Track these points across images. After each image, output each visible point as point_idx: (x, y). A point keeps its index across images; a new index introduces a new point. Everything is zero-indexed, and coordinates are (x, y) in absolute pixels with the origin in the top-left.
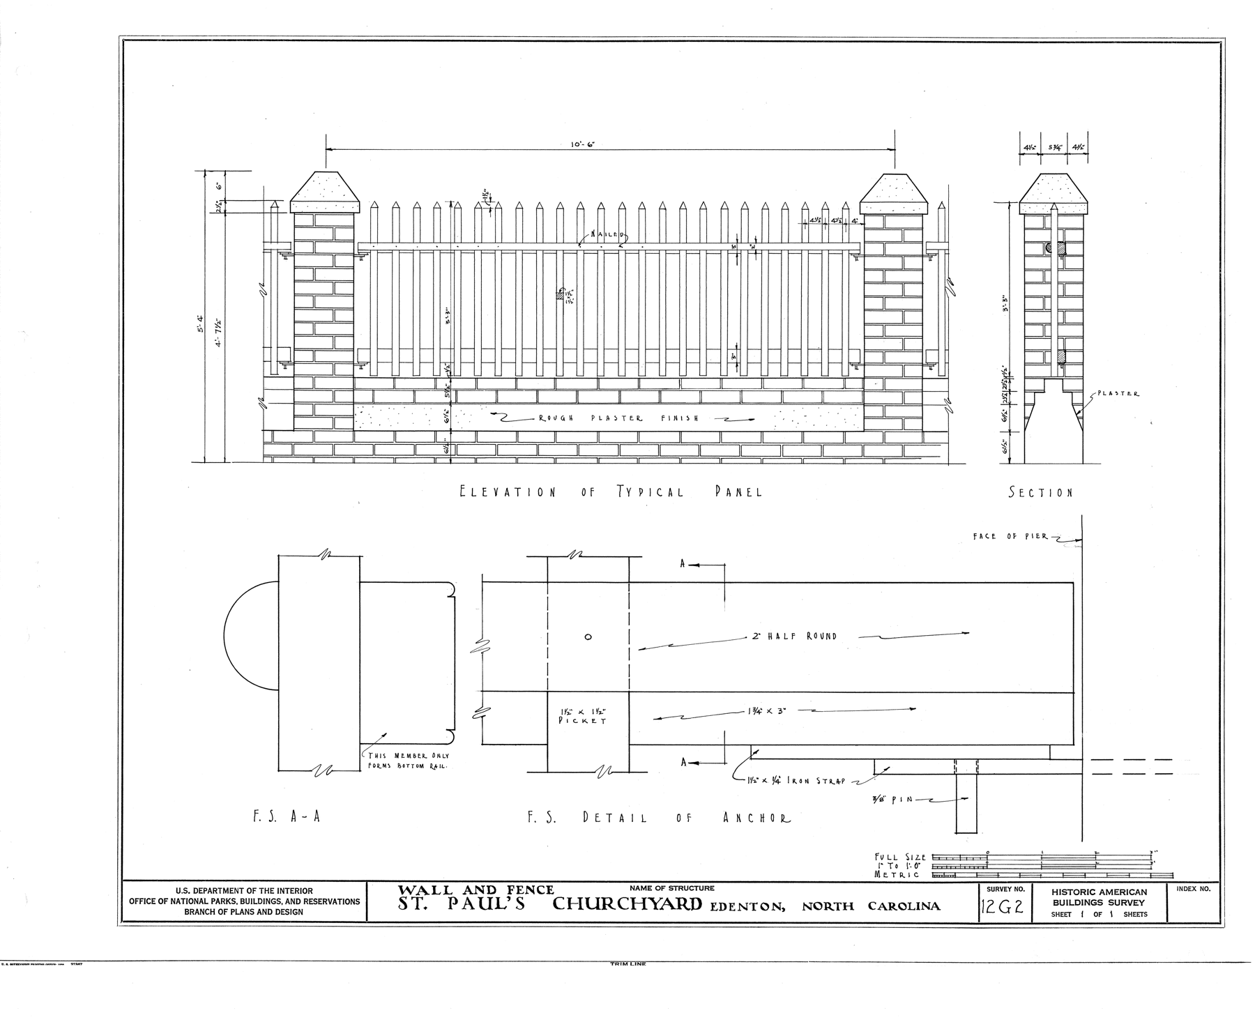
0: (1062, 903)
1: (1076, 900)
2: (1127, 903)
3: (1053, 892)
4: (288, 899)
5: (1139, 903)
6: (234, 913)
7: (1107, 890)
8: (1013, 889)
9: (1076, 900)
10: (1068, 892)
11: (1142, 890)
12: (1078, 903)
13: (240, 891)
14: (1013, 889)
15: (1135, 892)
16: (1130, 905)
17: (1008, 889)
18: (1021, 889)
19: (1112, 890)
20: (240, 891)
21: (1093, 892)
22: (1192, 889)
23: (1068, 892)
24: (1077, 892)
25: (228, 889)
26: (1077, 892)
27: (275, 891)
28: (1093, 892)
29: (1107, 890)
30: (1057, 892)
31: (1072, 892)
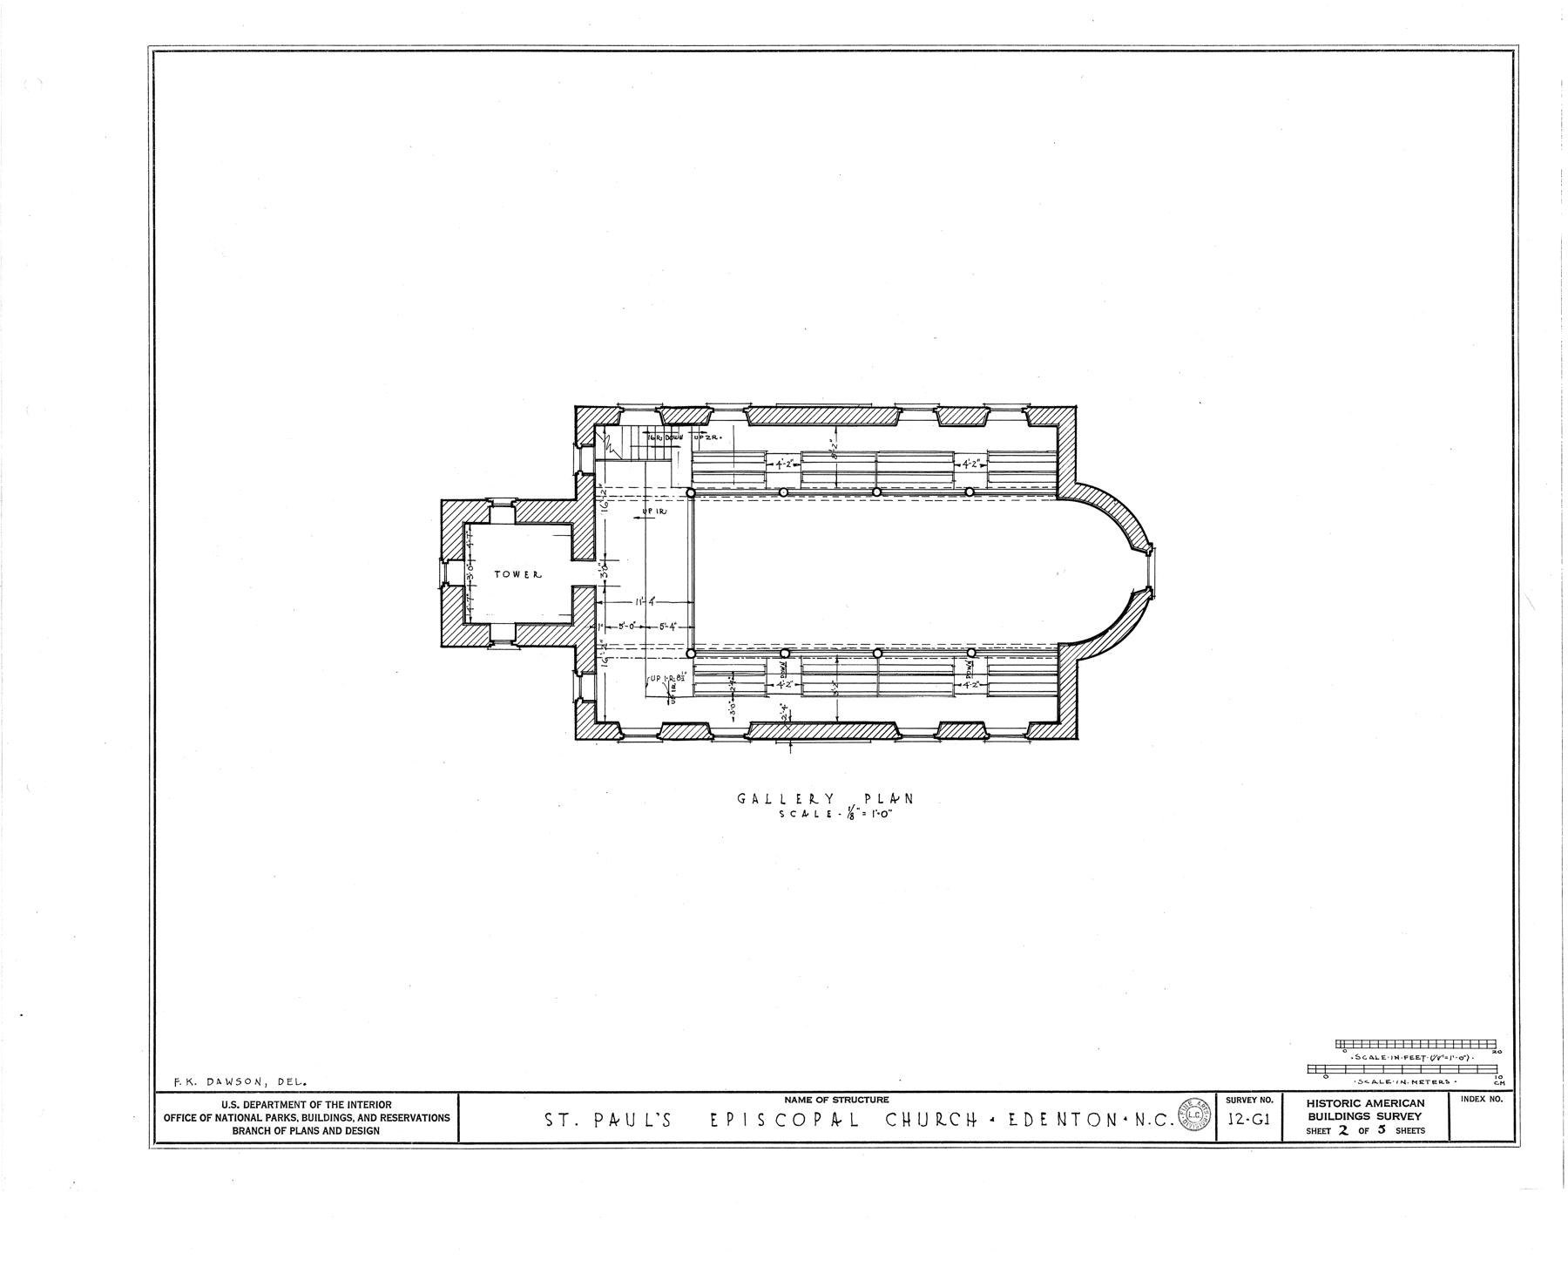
0: (1320, 1117)
4: (326, 1128)
5: (1415, 1117)
8: (1258, 1100)
10: (1327, 1103)
11: (1419, 1101)
12: (1339, 1116)
13: (301, 1104)
14: (1258, 1100)
15: (1410, 1103)
16: (1404, 1119)
17: (1252, 1100)
19: (1381, 1101)
20: (301, 1104)
21: (1357, 1103)
25: (286, 1102)
26: (1337, 1103)
28: (1357, 1103)
29: (1375, 1101)
30: (1313, 1103)
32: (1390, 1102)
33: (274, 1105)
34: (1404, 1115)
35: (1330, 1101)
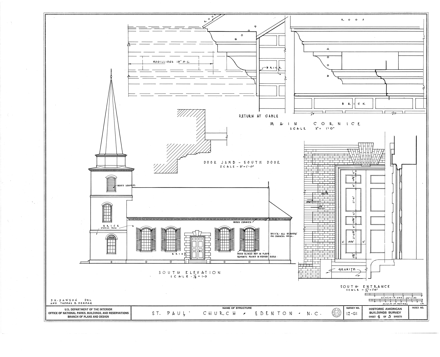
0: (373, 313)
2: (395, 313)
3: (369, 309)
5: (399, 313)
8: (355, 308)
10: (375, 309)
11: (400, 308)
12: (378, 313)
14: (355, 308)
15: (398, 309)
16: (396, 313)
18: (422, 308)
21: (383, 309)
24: (377, 309)
27: (99, 309)
28: (383, 309)
30: (371, 309)
32: (392, 309)
33: (79, 310)
34: (396, 312)
35: (375, 308)
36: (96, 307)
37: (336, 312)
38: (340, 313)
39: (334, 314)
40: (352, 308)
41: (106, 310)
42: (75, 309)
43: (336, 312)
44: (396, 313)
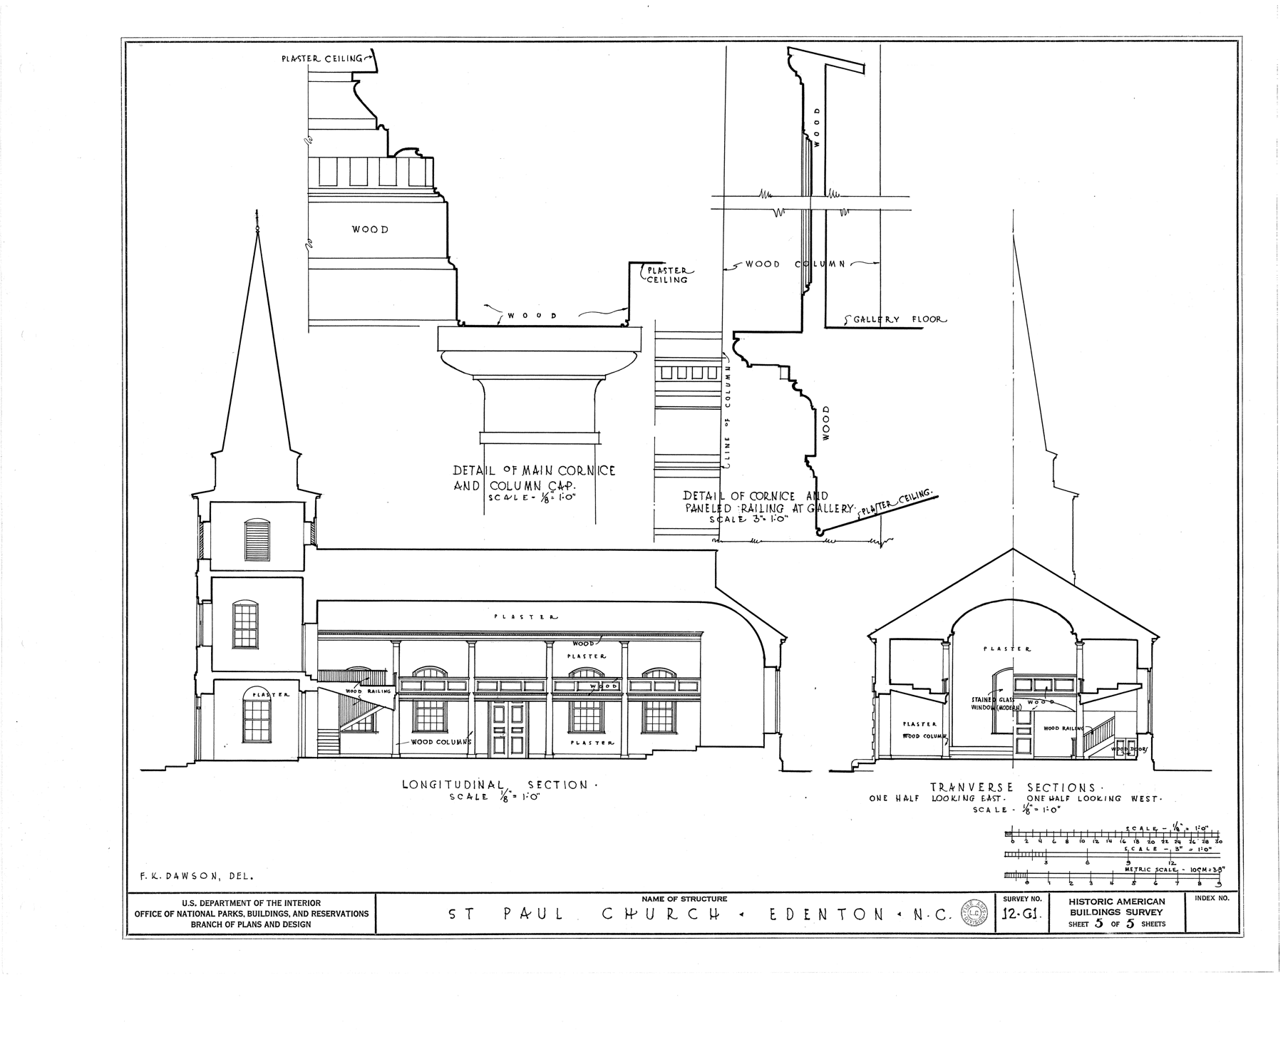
1: (1093, 910)
2: (1145, 913)
6: (241, 926)
7: (1125, 900)
8: (1029, 899)
9: (1093, 910)
10: (1086, 901)
14: (1029, 899)
15: (1153, 901)
16: (1148, 914)
17: (1025, 899)
19: (1129, 900)
21: (1110, 902)
22: (1211, 898)
23: (687, 899)
27: (283, 903)
28: (1110, 902)
29: (1125, 900)
30: (1074, 902)
31: (1089, 901)
33: (225, 903)
34: (1148, 911)
35: (1088, 900)
36: (275, 897)
37: (973, 913)
38: (986, 914)
39: (983, 914)
40: (1021, 899)
41: (302, 904)
42: (212, 902)
43: (973, 913)
44: (1148, 914)
